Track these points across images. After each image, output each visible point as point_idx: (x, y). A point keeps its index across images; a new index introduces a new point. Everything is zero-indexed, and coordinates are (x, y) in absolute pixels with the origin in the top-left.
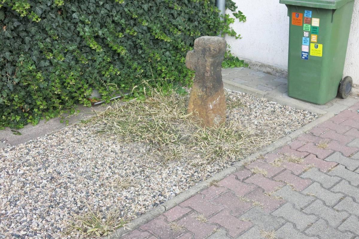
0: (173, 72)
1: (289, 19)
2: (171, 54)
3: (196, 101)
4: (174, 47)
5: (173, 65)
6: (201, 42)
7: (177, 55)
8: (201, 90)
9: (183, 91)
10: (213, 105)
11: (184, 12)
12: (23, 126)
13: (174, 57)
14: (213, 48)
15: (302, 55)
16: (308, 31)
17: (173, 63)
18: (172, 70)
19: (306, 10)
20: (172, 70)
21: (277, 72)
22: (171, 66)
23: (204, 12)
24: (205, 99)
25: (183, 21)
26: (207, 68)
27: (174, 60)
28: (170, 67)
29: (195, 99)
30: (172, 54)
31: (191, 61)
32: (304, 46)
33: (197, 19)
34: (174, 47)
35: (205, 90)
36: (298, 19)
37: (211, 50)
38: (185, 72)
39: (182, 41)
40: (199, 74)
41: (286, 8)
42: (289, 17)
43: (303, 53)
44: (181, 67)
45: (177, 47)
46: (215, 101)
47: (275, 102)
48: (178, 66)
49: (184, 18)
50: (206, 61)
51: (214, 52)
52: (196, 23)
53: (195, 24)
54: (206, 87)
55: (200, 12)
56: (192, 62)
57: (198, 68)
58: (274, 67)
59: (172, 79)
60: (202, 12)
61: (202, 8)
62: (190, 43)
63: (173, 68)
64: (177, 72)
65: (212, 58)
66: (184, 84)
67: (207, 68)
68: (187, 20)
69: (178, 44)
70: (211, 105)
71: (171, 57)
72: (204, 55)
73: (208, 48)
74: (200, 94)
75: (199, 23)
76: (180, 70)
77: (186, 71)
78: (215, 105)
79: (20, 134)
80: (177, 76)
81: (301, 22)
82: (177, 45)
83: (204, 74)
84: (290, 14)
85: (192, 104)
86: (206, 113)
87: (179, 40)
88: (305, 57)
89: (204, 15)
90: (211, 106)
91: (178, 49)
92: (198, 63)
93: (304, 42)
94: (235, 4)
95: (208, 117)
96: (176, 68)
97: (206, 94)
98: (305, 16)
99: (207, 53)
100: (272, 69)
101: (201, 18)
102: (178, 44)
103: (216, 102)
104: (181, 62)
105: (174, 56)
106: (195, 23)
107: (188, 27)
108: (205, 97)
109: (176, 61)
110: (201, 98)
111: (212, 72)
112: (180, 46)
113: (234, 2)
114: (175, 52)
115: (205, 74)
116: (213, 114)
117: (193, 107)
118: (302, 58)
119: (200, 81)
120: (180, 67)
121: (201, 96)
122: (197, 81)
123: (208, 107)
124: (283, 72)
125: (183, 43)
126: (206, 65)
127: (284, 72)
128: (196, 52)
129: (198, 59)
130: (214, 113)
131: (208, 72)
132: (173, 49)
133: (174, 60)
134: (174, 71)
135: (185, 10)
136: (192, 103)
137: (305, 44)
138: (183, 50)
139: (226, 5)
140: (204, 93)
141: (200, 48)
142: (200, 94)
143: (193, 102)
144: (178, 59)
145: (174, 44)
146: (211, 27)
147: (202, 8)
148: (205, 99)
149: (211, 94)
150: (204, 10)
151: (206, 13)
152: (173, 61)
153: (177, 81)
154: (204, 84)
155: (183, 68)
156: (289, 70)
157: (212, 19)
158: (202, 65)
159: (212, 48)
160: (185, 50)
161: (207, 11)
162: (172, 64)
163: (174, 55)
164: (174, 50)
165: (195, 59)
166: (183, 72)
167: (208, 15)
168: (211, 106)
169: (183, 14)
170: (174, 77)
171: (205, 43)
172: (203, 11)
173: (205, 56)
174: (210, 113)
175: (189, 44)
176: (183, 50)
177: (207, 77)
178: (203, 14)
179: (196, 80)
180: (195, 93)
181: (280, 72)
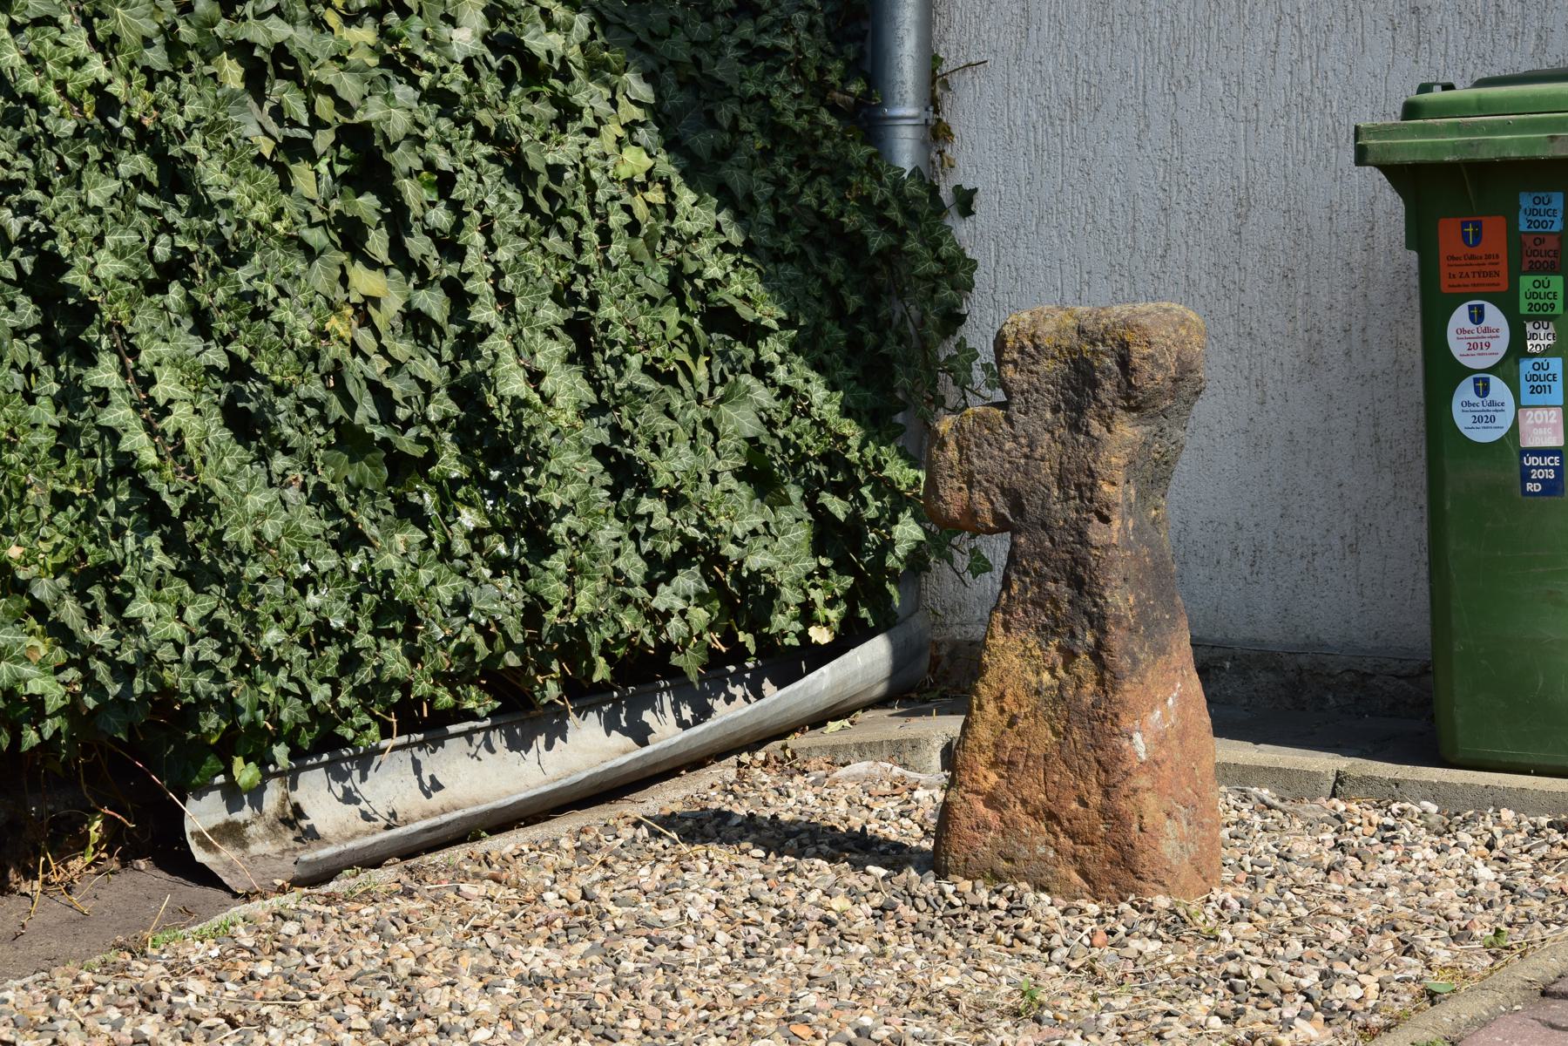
1: (1415, 266)
10: (1149, 735)
12: (297, 839)
15: (1526, 475)
16: (1550, 318)
19: (1530, 191)
26: (1106, 488)
32: (1530, 412)
36: (1477, 251)
37: (1136, 361)
41: (1390, 205)
42: (1414, 255)
43: (1532, 461)
67: (1106, 488)
70: (1137, 737)
73: (768, 585)
79: (1185, 370)
81: (1503, 267)
84: (1419, 234)
86: (1107, 794)
88: (1543, 482)
93: (1534, 390)
98: (1523, 227)
103: (1164, 718)
111: (1131, 524)
118: (1525, 493)
123: (1118, 750)
126: (1098, 467)
137: (1537, 399)
154: (1087, 603)
156: (1434, 635)
171: (1081, 331)
177: (1106, 548)
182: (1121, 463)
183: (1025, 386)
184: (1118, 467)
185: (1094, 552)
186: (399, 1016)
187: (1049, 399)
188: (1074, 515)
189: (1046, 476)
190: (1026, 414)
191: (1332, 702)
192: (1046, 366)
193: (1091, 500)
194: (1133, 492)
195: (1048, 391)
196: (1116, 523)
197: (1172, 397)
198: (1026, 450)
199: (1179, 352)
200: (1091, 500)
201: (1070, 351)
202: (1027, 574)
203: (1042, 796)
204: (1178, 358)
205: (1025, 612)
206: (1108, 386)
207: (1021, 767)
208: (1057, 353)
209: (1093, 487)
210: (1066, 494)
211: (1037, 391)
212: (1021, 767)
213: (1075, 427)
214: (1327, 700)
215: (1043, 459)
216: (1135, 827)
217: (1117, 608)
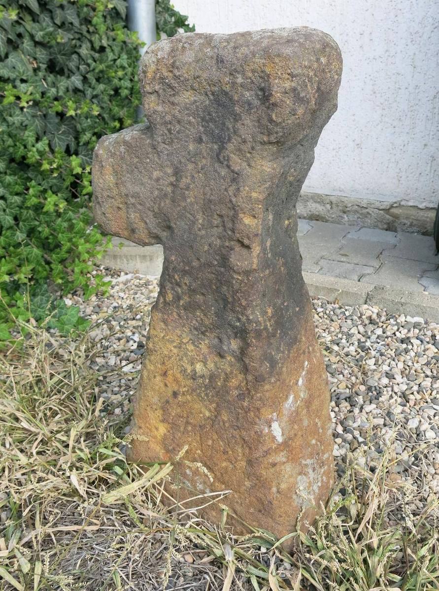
0: (24, 251)
2: (5, 187)
3: (181, 405)
4: (12, 160)
5: (17, 225)
6: (189, 57)
7: (27, 189)
8: (204, 348)
9: (72, 317)
10: (285, 419)
11: (32, 37)
13: (16, 198)
14: (287, 85)
17: (16, 219)
18: (19, 245)
20: (19, 245)
21: (344, 212)
22: (11, 228)
23: (97, 45)
24: (241, 397)
25: (30, 67)
26: (247, 221)
27: (21, 208)
28: (9, 233)
29: (175, 394)
30: (9, 184)
31: (131, 188)
33: (78, 68)
34: (12, 160)
35: (235, 345)
37: (277, 96)
38: (67, 246)
39: (38, 140)
40: (189, 263)
44: (47, 230)
45: (24, 158)
46: (291, 398)
47: (418, 314)
48: (36, 226)
49: (35, 59)
50: (236, 177)
51: (293, 112)
52: (76, 81)
53: (73, 83)
54: (242, 333)
55: (84, 46)
56: (136, 196)
57: (180, 225)
58: (333, 199)
59: (22, 276)
60: (89, 45)
61: (88, 31)
62: (66, 143)
63: (20, 236)
64: (38, 247)
65: (275, 157)
66: (69, 288)
67: (247, 221)
68: (43, 66)
69: (25, 147)
70: (275, 426)
71: (8, 196)
72: (221, 141)
74: (199, 367)
75: (85, 80)
76: (47, 238)
77: (70, 240)
78: (295, 418)
80: (38, 263)
82: (21, 151)
83: (224, 261)
85: (154, 417)
86: (250, 463)
87: (27, 133)
89: (97, 55)
90: (277, 430)
91: (28, 166)
92: (177, 192)
94: (186, 18)
95: (261, 484)
96: (31, 232)
97: (246, 370)
99: (247, 126)
100: (328, 206)
101: (88, 65)
102: (25, 147)
104: (45, 210)
105: (17, 194)
106: (73, 78)
107: (54, 90)
108: (234, 382)
109: (28, 208)
110: (213, 387)
111: (268, 244)
112: (33, 156)
113: (182, 13)
114: (20, 178)
115: (233, 259)
116: (288, 468)
117: (162, 429)
119: (199, 298)
120: (45, 231)
121: (212, 377)
122: (178, 298)
123: (259, 435)
124: (365, 211)
125: (42, 145)
126: (239, 201)
127: (369, 210)
128: (161, 130)
129: (177, 173)
130: (293, 459)
131: (248, 247)
132: (8, 168)
133: (21, 208)
134: (27, 245)
135: (34, 32)
136: (159, 413)
138: (46, 166)
139: (157, 28)
140: (228, 364)
141: (186, 97)
142: (199, 367)
143: (164, 409)
144: (34, 201)
145: (11, 150)
146: (125, 92)
147: (88, 31)
148: (241, 397)
149: (273, 363)
150: (95, 38)
151: (102, 49)
152: (16, 211)
153: (42, 281)
154: (231, 317)
155: (54, 230)
157: (123, 68)
158: (207, 206)
159: (280, 87)
160: (55, 166)
161: (105, 43)
162: (13, 222)
163: (19, 188)
164: (14, 174)
165: (156, 174)
166: (58, 246)
167: (111, 56)
168: (277, 430)
169: (27, 44)
170: (31, 267)
171: (220, 60)
172: (91, 42)
173: (230, 146)
174: (274, 465)
175: (64, 148)
176: (46, 166)
177: (247, 273)
178: (93, 53)
179: (170, 297)
180: (169, 364)
181: (356, 212)
182: (261, 197)
183: (168, 118)
184: (258, 201)
185: (235, 276)
186: (82, 241)
187: (192, 132)
188: (218, 242)
189: (192, 204)
190: (171, 143)
191: (346, 218)
192: (186, 97)
193: (233, 231)
194: (271, 217)
195: (190, 122)
196: (256, 249)
197: (310, 127)
198: (173, 179)
199: (319, 83)
200: (233, 231)
201: (211, 83)
202: (178, 285)
203: (199, 452)
204: (319, 89)
205: (179, 315)
206: (248, 122)
207: (182, 429)
208: (196, 85)
209: (234, 218)
210: (210, 222)
211: (179, 122)
212: (182, 429)
213: (219, 158)
214: (344, 218)
215: (188, 188)
216: (274, 489)
217: (258, 323)
